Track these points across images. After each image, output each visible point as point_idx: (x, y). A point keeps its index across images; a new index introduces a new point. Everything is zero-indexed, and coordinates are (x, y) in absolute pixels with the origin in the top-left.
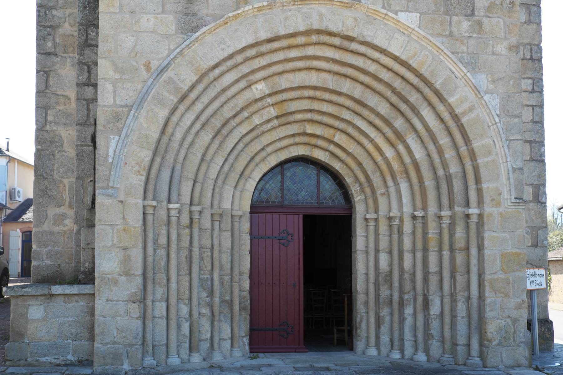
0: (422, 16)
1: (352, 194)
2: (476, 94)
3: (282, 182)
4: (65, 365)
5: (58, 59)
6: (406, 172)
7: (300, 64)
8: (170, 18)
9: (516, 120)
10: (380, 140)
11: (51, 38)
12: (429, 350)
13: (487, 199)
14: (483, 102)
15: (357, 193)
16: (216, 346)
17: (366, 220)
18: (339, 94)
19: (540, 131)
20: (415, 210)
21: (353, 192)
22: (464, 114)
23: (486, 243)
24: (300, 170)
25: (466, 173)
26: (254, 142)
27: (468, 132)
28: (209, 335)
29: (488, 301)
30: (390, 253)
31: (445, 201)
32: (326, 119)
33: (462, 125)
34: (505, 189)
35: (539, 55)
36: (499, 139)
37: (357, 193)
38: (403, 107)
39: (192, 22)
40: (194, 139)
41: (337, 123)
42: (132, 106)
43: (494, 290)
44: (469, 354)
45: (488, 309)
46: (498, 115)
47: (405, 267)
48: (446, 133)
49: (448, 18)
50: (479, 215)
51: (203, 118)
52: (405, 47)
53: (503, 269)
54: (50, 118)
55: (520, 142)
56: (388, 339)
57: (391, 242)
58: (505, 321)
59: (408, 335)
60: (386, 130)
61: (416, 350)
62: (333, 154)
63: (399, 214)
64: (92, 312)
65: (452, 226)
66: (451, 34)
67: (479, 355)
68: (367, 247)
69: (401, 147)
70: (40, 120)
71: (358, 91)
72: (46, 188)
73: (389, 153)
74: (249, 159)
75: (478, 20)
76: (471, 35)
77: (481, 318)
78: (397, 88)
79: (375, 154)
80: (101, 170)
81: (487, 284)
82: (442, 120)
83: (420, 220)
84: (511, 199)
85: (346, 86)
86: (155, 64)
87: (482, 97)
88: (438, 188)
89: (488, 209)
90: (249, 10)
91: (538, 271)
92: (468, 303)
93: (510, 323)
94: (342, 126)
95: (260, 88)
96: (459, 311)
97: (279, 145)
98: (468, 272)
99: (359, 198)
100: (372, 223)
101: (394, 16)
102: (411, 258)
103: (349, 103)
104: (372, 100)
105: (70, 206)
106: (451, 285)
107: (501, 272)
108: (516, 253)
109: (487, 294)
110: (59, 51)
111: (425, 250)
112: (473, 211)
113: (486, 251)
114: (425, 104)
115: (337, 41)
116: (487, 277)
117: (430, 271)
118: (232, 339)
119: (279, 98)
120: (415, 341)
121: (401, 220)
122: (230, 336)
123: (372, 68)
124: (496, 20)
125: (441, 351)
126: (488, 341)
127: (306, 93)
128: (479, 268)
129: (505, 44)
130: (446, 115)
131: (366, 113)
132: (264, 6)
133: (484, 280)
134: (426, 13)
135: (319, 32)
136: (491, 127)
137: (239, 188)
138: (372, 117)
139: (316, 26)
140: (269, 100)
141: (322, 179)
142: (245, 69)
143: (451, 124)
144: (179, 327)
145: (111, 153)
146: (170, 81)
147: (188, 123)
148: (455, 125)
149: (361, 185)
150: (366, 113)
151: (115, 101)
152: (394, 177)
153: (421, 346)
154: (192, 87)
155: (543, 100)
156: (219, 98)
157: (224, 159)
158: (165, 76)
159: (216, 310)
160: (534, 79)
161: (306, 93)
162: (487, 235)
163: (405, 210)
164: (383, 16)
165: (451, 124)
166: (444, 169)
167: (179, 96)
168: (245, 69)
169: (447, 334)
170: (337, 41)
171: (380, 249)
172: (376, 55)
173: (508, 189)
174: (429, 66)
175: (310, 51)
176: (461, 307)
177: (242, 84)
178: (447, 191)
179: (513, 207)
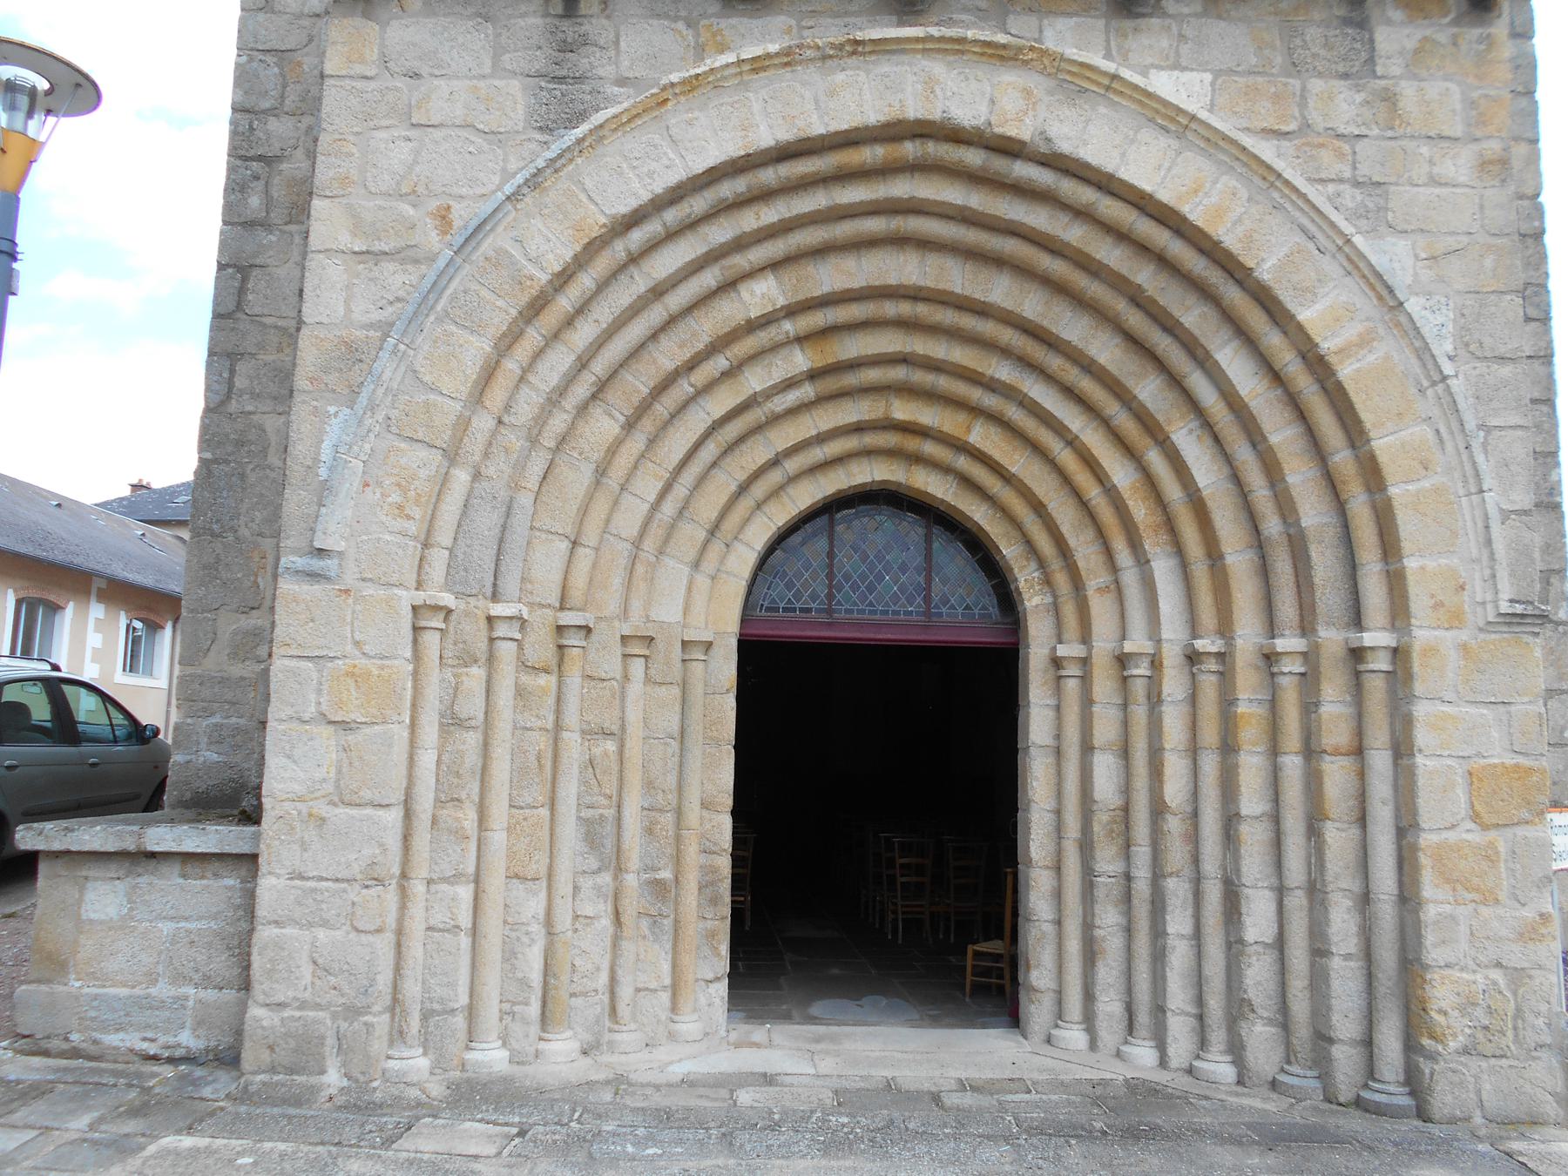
0: (1220, 81)
1: (1017, 588)
2: (1380, 298)
3: (831, 555)
4: (171, 1061)
5: (273, 238)
7: (875, 225)
8: (515, 86)
10: (1094, 440)
11: (260, 185)
12: (1243, 1047)
13: (1419, 601)
14: (1403, 319)
15: (1032, 587)
16: (624, 1010)
17: (1057, 662)
19: (1546, 426)
20: (1195, 636)
21: (1022, 584)
23: (1422, 737)
24: (881, 529)
25: (1352, 526)
26: (749, 443)
27: (1359, 406)
28: (603, 978)
29: (1430, 913)
30: (1125, 753)
31: (1287, 609)
32: (943, 383)
33: (1339, 386)
34: (1477, 575)
35: (1536, 224)
36: (1455, 425)
37: (1032, 587)
39: (572, 101)
40: (573, 426)
41: (976, 395)
42: (392, 324)
43: (1447, 878)
44: (1371, 1072)
45: (1430, 938)
46: (1450, 358)
47: (1167, 799)
48: (1288, 414)
49: (1295, 83)
50: (1395, 651)
51: (600, 367)
52: (1169, 169)
53: (1475, 817)
54: (240, 382)
55: (1519, 433)
56: (1118, 1004)
57: (1126, 724)
58: (1486, 978)
59: (1178, 996)
60: (1112, 408)
61: (1203, 1044)
62: (967, 482)
63: (1148, 647)
65: (1310, 680)
66: (1306, 126)
67: (1402, 1078)
68: (1058, 737)
69: (1154, 458)
70: (216, 387)
71: (1032, 304)
72: (218, 560)
73: (1121, 475)
74: (733, 487)
75: (1386, 89)
76: (1364, 131)
77: (1411, 966)
78: (1145, 286)
79: (1083, 478)
81: (1424, 860)
83: (1213, 666)
84: (1496, 602)
85: (1000, 290)
87: (1401, 304)
88: (1264, 571)
89: (1422, 635)
90: (727, 66)
92: (1363, 912)
93: (1502, 982)
94: (990, 401)
95: (763, 294)
96: (1335, 939)
98: (1362, 820)
99: (1036, 600)
100: (1072, 670)
101: (1136, 79)
102: (1185, 771)
103: (1007, 336)
104: (1072, 328)
106: (1309, 856)
107: (1472, 826)
108: (1517, 766)
109: (1428, 891)
110: (277, 217)
111: (1228, 748)
112: (1376, 637)
113: (1419, 760)
114: (1226, 332)
115: (973, 157)
116: (1427, 840)
117: (1244, 812)
118: (675, 989)
119: (818, 319)
120: (1200, 1018)
121: (1156, 663)
122: (667, 981)
123: (1074, 234)
125: (1277, 1055)
126: (1432, 1037)
127: (891, 309)
128: (1397, 809)
131: (1055, 363)
132: (768, 56)
133: (1414, 848)
136: (1430, 392)
137: (709, 565)
138: (1073, 375)
140: (788, 327)
141: (936, 545)
142: (720, 233)
143: (1304, 383)
144: (510, 955)
146: (499, 259)
147: (554, 379)
148: (1315, 387)
149: (1042, 564)
150: (1055, 363)
151: (348, 310)
152: (1135, 544)
153: (1218, 1037)
154: (564, 278)
155: (1550, 342)
156: (645, 314)
157: (660, 485)
158: (487, 246)
159: (630, 908)
161: (891, 309)
162: (1421, 710)
163: (1166, 634)
164: (1106, 81)
165: (1304, 383)
166: (1284, 518)
167: (525, 299)
168: (720, 233)
169: (1300, 1007)
170: (973, 157)
171: (1096, 743)
172: (1086, 195)
173: (1487, 572)
174: (1239, 221)
175: (901, 188)
176: (1342, 922)
177: (709, 278)
178: (1292, 579)
179: (1505, 629)
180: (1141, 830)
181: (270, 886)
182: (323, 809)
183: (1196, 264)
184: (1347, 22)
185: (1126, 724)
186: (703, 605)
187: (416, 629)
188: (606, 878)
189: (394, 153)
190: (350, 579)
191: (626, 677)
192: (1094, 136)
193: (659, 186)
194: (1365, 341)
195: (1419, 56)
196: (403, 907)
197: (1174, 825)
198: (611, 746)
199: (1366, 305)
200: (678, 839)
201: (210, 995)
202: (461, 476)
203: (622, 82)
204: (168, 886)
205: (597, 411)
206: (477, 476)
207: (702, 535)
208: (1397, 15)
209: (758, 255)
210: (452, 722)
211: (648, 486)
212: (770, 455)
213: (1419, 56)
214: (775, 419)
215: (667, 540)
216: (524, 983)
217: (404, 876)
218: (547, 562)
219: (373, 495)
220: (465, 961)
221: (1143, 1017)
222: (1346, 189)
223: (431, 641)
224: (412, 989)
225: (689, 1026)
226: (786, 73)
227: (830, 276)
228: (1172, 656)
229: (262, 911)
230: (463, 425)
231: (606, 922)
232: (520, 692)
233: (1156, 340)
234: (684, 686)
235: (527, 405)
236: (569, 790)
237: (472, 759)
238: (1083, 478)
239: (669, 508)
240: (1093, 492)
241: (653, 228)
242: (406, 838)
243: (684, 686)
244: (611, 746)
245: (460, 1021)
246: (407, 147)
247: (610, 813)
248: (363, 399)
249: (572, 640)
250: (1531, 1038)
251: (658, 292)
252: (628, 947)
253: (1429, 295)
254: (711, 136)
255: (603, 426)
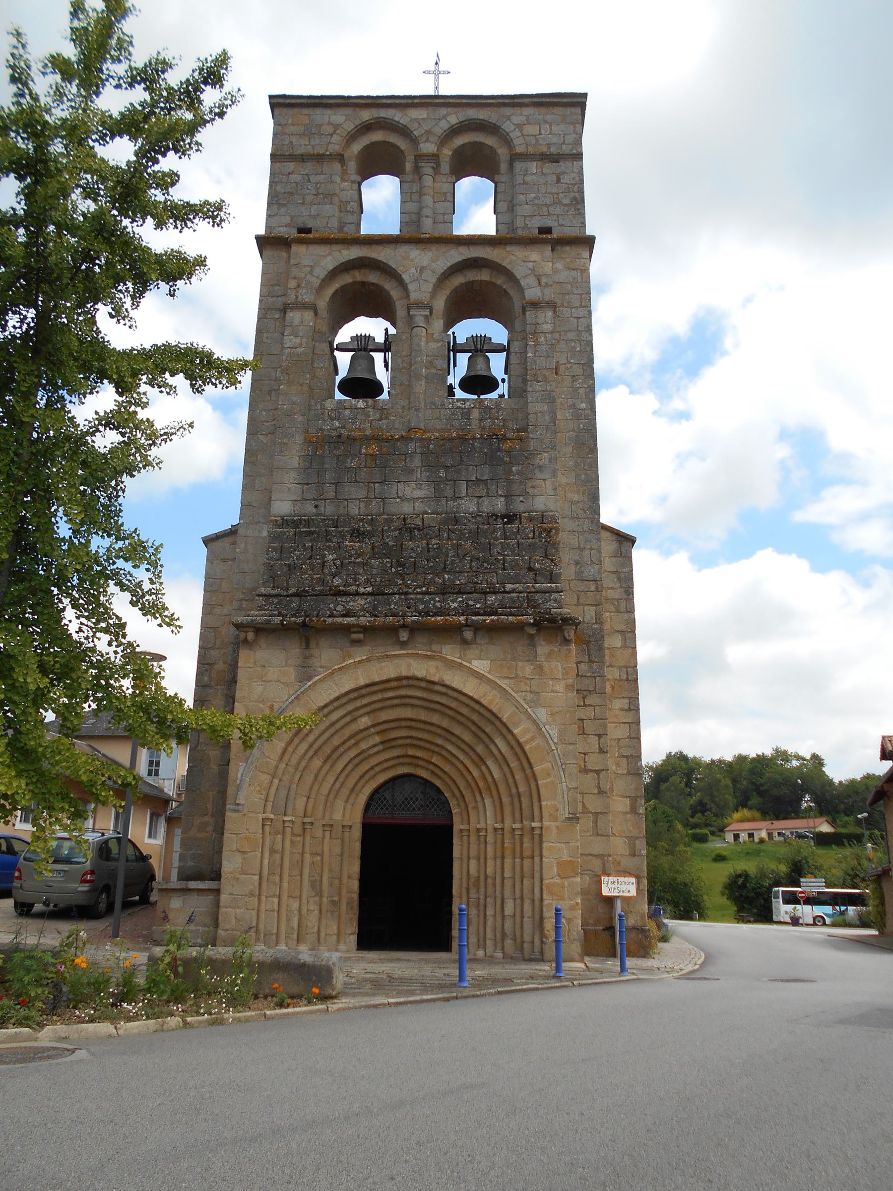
6: (489, 788)
7: (396, 701)
8: (291, 669)
9: (571, 747)
10: (467, 762)
11: (207, 673)
16: (322, 940)
18: (432, 724)
22: (527, 742)
28: (316, 929)
30: (479, 860)
31: (517, 815)
32: (422, 744)
38: (482, 736)
43: (551, 894)
51: (315, 747)
53: (559, 875)
57: (479, 850)
62: (433, 773)
64: (217, 905)
66: (517, 676)
71: (445, 723)
73: (476, 773)
74: (358, 777)
79: (465, 773)
80: (230, 790)
82: (512, 748)
85: (435, 719)
86: (276, 706)
91: (626, 879)
94: (437, 749)
95: (364, 722)
97: (386, 765)
101: (468, 665)
105: (212, 816)
116: (545, 882)
118: (338, 935)
119: (382, 727)
122: (336, 932)
123: (454, 705)
124: (555, 663)
129: (563, 683)
130: (513, 743)
131: (454, 739)
134: (495, 660)
135: (408, 678)
137: (351, 801)
138: (459, 743)
139: (404, 674)
140: (372, 730)
142: (350, 707)
145: (239, 776)
153: (499, 945)
159: (324, 909)
160: (630, 698)
161: (404, 724)
168: (350, 707)
170: (423, 684)
175: (403, 692)
177: (348, 719)
180: (482, 883)
181: (224, 897)
182: (238, 876)
183: (488, 715)
184: (529, 645)
185: (479, 850)
186: (350, 813)
187: (263, 825)
188: (317, 899)
189: (258, 689)
190: (245, 811)
191: (324, 836)
192: (455, 680)
193: (332, 698)
194: (533, 739)
195: (549, 655)
196: (259, 904)
197: (490, 881)
198: (319, 858)
199: (533, 728)
200: (340, 888)
201: (206, 929)
202: (276, 781)
203: (321, 667)
204: (194, 899)
205: (315, 758)
206: (280, 780)
207: (348, 792)
208: (543, 643)
209: (362, 711)
210: (273, 851)
211: (331, 779)
212: (369, 766)
213: (549, 655)
214: (370, 756)
215: (337, 794)
216: (293, 928)
217: (259, 895)
218: (300, 803)
219: (252, 788)
220: (276, 920)
221: (481, 942)
222: (528, 694)
223: (267, 828)
224: (261, 926)
225: (342, 947)
226: (368, 663)
227: (384, 716)
228: (490, 830)
229: (221, 904)
230: (277, 767)
231: (317, 912)
232: (292, 842)
233: (480, 734)
234: (343, 840)
235: (294, 761)
236: (306, 871)
237: (278, 862)
238: (465, 773)
239: (337, 785)
240: (469, 778)
241: (331, 708)
242: (260, 884)
243: (343, 840)
244: (319, 858)
245: (274, 937)
246: (262, 687)
247: (318, 879)
248: (250, 761)
249: (308, 826)
250: (572, 938)
251: (333, 724)
252: (324, 921)
253: (551, 725)
254: (347, 683)
255: (317, 763)
